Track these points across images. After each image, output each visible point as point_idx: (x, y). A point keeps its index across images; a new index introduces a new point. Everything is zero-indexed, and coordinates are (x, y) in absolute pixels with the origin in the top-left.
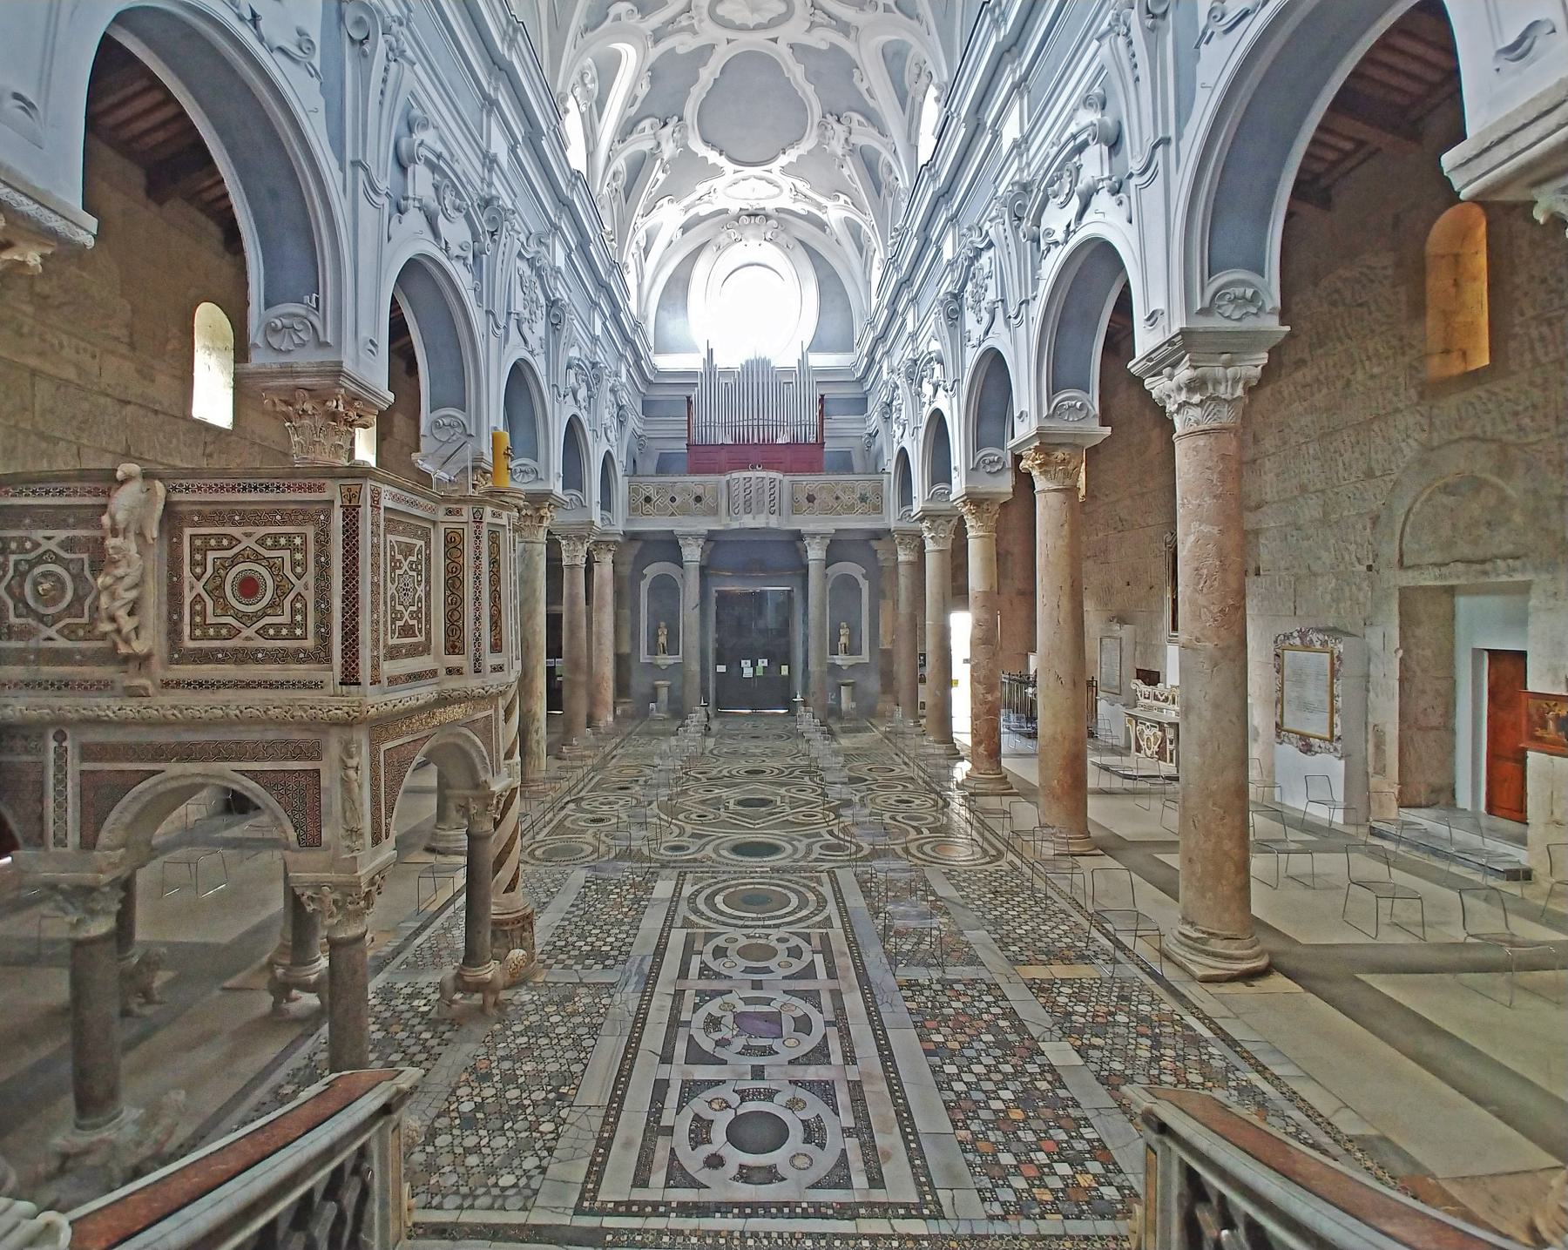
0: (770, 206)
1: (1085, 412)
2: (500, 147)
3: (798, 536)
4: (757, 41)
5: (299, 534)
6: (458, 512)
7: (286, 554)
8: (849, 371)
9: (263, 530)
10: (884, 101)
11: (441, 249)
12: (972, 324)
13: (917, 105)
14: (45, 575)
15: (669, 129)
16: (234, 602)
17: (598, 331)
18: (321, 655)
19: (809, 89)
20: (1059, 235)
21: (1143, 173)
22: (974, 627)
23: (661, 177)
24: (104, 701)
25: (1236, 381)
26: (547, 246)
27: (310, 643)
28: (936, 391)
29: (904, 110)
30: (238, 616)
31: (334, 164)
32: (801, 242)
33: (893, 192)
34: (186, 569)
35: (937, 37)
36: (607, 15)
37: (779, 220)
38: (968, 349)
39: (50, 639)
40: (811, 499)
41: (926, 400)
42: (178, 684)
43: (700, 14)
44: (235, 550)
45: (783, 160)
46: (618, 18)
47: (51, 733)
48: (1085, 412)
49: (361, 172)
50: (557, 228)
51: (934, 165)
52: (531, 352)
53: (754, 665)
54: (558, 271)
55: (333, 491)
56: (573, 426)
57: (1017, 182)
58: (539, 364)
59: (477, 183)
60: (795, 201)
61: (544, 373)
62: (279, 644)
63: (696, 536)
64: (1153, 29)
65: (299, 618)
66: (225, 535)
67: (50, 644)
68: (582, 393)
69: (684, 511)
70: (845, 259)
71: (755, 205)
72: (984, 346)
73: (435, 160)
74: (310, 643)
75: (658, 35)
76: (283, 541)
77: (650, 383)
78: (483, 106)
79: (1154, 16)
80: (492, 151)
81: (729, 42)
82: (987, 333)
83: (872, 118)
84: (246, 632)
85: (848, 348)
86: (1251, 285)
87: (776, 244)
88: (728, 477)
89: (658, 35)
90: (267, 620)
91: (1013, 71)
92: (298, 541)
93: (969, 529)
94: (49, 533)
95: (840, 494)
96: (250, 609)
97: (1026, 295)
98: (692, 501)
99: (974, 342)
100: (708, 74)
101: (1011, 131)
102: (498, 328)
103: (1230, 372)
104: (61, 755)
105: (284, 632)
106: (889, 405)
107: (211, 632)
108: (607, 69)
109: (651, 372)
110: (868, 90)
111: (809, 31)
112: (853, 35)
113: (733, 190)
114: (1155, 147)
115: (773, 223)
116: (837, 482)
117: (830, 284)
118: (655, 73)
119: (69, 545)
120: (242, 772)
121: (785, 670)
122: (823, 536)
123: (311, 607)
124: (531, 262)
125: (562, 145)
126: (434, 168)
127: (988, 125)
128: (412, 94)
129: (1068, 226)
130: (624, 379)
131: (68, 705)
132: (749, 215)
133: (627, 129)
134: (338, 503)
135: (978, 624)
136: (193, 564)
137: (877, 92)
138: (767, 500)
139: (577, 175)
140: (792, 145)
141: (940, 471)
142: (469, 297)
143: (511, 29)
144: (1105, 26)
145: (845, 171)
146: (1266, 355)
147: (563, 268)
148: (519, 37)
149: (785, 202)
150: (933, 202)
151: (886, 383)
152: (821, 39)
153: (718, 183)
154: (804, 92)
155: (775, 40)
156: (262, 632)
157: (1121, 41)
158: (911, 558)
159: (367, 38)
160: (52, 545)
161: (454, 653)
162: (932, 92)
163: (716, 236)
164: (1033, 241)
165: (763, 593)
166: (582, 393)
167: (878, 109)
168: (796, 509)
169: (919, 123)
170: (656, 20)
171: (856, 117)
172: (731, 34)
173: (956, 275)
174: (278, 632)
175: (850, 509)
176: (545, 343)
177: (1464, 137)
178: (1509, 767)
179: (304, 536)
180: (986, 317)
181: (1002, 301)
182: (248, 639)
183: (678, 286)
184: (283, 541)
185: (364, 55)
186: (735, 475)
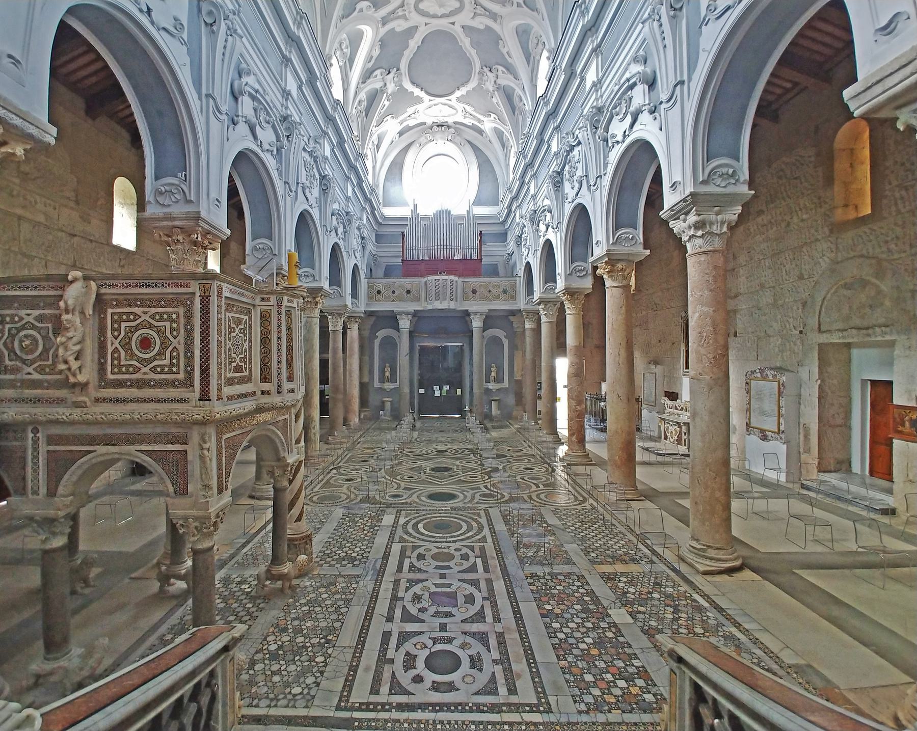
0: (450, 120)
1: (634, 241)
2: (292, 86)
3: (467, 313)
4: (443, 24)
5: (175, 313)
6: (268, 300)
8: (496, 217)
9: (154, 310)
11: (258, 146)
13: (536, 62)
15: (391, 75)
16: (137, 352)
17: (350, 194)
18: (188, 383)
19: (473, 52)
20: (619, 138)
21: (668, 101)
22: (570, 367)
23: (387, 103)
24: (61, 410)
25: (723, 223)
26: (320, 144)
27: (181, 376)
28: (547, 229)
29: (528, 64)
30: (139, 360)
31: (196, 96)
32: (469, 142)
33: (522, 112)
34: (109, 332)
35: (548, 22)
36: (355, 9)
37: (456, 129)
38: (566, 204)
39: (29, 374)
40: (474, 292)
41: (542, 234)
42: (104, 400)
44: (138, 322)
45: (458, 94)
46: (361, 10)
47: (30, 428)
48: (634, 241)
50: (326, 133)
51: (546, 96)
54: (327, 158)
55: (195, 287)
56: (335, 249)
57: (594, 107)
58: (315, 213)
59: (279, 107)
60: (465, 117)
61: (318, 218)
62: (163, 376)
63: (407, 314)
65: (175, 361)
66: (131, 313)
67: (29, 377)
68: (341, 230)
69: (400, 299)
70: (494, 152)
71: (441, 120)
72: (576, 202)
73: (254, 93)
74: (181, 376)
75: (385, 20)
76: (165, 316)
77: (380, 224)
78: (283, 62)
79: (675, 10)
81: (426, 24)
82: (577, 194)
83: (510, 69)
84: (144, 370)
85: (496, 204)
86: (731, 167)
87: (454, 143)
88: (426, 279)
89: (385, 20)
90: (156, 363)
91: (593, 42)
92: (174, 316)
93: (567, 310)
94: (29, 312)
95: (491, 289)
96: (146, 356)
97: (600, 172)
98: (404, 293)
99: (570, 200)
100: (414, 43)
101: (591, 77)
102: (291, 192)
103: (719, 217)
104: (36, 441)
105: (166, 369)
106: (520, 237)
108: (355, 41)
109: (381, 218)
110: (508, 53)
111: (473, 18)
112: (499, 20)
113: (429, 111)
114: (676, 86)
115: (452, 130)
116: (489, 282)
117: (485, 166)
118: (383, 43)
119: (40, 319)
120: (142, 452)
121: (459, 392)
122: (482, 313)
123: (182, 355)
124: (311, 153)
125: (329, 85)
126: (254, 98)
127: (578, 73)
128: (241, 55)
129: (625, 132)
130: (365, 222)
131: (40, 412)
132: (438, 126)
133: (367, 75)
134: (198, 294)
135: (572, 365)
136: (113, 330)
137: (513, 54)
138: (449, 292)
139: (337, 102)
140: (463, 85)
141: (550, 276)
142: (274, 174)
143: (299, 17)
144: (646, 15)
145: (494, 100)
146: (741, 208)
147: (329, 157)
149: (459, 118)
150: (546, 118)
151: (518, 224)
152: (480, 23)
153: (420, 107)
154: (470, 54)
155: (453, 24)
156: (153, 370)
158: (533, 326)
160: (30, 319)
161: (265, 382)
162: (545, 54)
163: (419, 138)
165: (446, 347)
166: (341, 230)
167: (513, 63)
168: (465, 298)
169: (537, 72)
170: (384, 12)
171: (501, 68)
172: (427, 20)
173: (559, 161)
174: (163, 370)
175: (497, 297)
176: (319, 201)
177: (856, 80)
179: (178, 314)
180: (577, 186)
181: (586, 176)
182: (145, 373)
183: (396, 167)
184: (165, 316)
185: (213, 32)
186: (430, 278)
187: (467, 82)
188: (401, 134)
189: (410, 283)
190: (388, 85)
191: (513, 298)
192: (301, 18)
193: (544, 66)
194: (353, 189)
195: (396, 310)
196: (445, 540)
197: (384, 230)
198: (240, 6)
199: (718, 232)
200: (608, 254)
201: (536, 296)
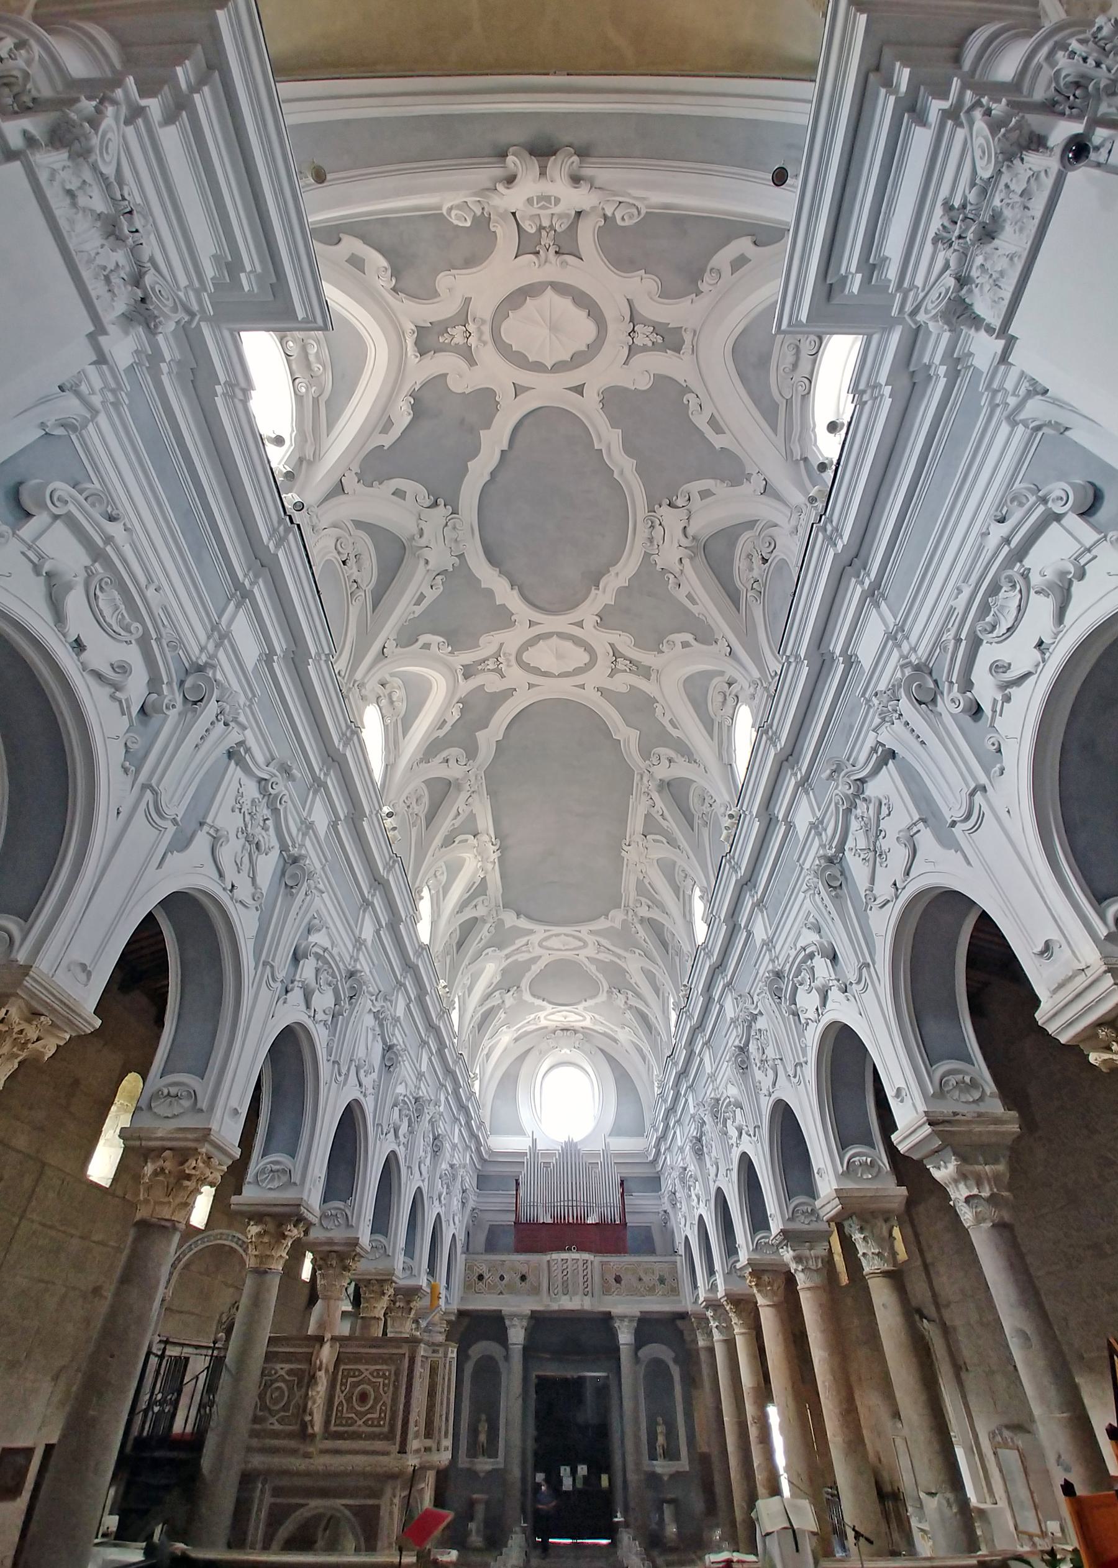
1: (876, 1169)
2: (368, 932)
3: (607, 1318)
7: (381, 1380)
8: (646, 1152)
10: (666, 894)
11: (309, 1017)
12: (807, 1001)
13: (687, 898)
15: (510, 993)
17: (424, 1068)
18: (389, 1437)
19: (600, 976)
21: (968, 817)
23: (503, 1016)
24: (292, 1460)
26: (391, 1002)
28: (741, 1134)
29: (658, 997)
30: (357, 1413)
31: (252, 964)
32: (602, 1050)
33: (679, 952)
34: (338, 1387)
35: (694, 859)
36: (417, 640)
37: (583, 1033)
38: (762, 1097)
40: (618, 1280)
41: (733, 1141)
43: (508, 660)
44: (360, 1378)
47: (261, 1478)
48: (876, 1169)
49: (336, 1066)
50: (401, 985)
51: (771, 726)
52: (365, 1096)
53: (574, 1472)
54: (398, 1020)
55: (405, 1350)
56: (390, 1167)
58: (369, 1105)
59: (347, 958)
61: (372, 1109)
63: (520, 1317)
64: (837, 896)
65: (383, 1415)
67: (272, 1427)
68: (404, 1129)
69: (511, 1289)
70: (634, 1065)
71: (566, 1025)
73: (100, 543)
74: (386, 1429)
75: (507, 957)
77: (485, 1161)
78: (362, 905)
79: (835, 888)
80: (363, 937)
82: (774, 1084)
83: (638, 995)
84: (360, 1422)
85: (640, 1132)
86: (867, 1156)
87: (583, 1051)
88: (548, 1257)
89: (507, 957)
90: (369, 1416)
91: (665, 1144)
93: (735, 1326)
95: (643, 1276)
96: (363, 1409)
97: (799, 1059)
98: (518, 1280)
99: (765, 1091)
101: (760, 933)
102: (274, 980)
104: (262, 1492)
106: (699, 1140)
107: (344, 1422)
108: (454, 870)
109: (486, 1152)
110: (671, 721)
112: (653, 676)
113: (551, 1017)
114: (972, 794)
115: (580, 1036)
116: (639, 1263)
117: (624, 1081)
118: (504, 972)
119: (290, 1372)
121: (605, 1480)
122: (631, 1318)
125: (415, 920)
126: (318, 957)
127: (780, 818)
128: (317, 912)
129: (817, 1009)
130: (442, 1109)
131: (276, 1461)
132: (562, 1030)
133: (487, 997)
134: (407, 1355)
136: (342, 1384)
138: (581, 1280)
139: (423, 947)
141: (758, 1220)
142: (321, 1053)
143: (281, 528)
144: (727, 1058)
147: (369, 943)
148: (424, 952)
149: (587, 1023)
150: (776, 769)
151: (693, 1116)
152: (623, 682)
153: (542, 1014)
155: (582, 687)
157: (898, 725)
159: (201, 700)
162: (697, 892)
164: (794, 1014)
165: (582, 1379)
166: (404, 1129)
168: (606, 1291)
169: (820, 364)
170: (467, 657)
172: (550, 952)
173: (740, 1031)
175: (651, 1290)
176: (376, 1087)
177: (897, 1129)
178: (890, 1504)
179: (390, 1371)
180: (770, 1073)
181: (781, 1059)
182: (360, 1426)
183: (509, 1081)
185: (292, 894)
186: (555, 1256)
188: (516, 1040)
189: (527, 1262)
190: (506, 1001)
191: (675, 1291)
192: (394, 862)
193: (699, 907)
195: (506, 1310)
197: (492, 1170)
198: (254, 696)
199: (814, 1267)
200: (750, 1263)
201: (776, 1226)
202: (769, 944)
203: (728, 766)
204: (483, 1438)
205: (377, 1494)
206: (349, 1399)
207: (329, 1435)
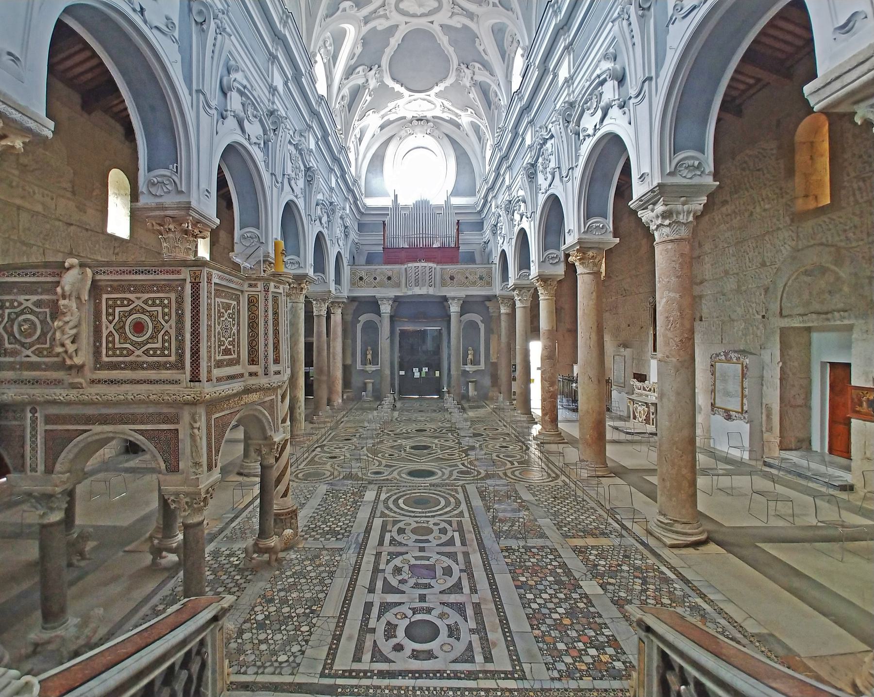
0: (429, 115)
1: (605, 230)
2: (278, 82)
3: (445, 299)
4: (422, 23)
5: (166, 298)
6: (256, 286)
8: (473, 207)
9: (146, 296)
10: (493, 56)
13: (511, 59)
14: (25, 321)
15: (373, 72)
16: (130, 336)
17: (334, 185)
18: (179, 365)
19: (451, 50)
20: (590, 131)
21: (637, 96)
22: (543, 350)
23: (369, 98)
24: (58, 391)
25: (689, 212)
26: (305, 137)
27: (173, 359)
28: (522, 218)
29: (504, 61)
30: (133, 343)
31: (186, 92)
32: (447, 135)
33: (498, 107)
34: (104, 317)
35: (522, 21)
36: (339, 8)
37: (434, 123)
38: (540, 195)
39: (28, 356)
40: (452, 278)
41: (516, 223)
42: (99, 381)
43: (390, 8)
44: (131, 307)
45: (437, 89)
46: (344, 10)
47: (28, 409)
48: (605, 230)
49: (201, 96)
50: (311, 127)
51: (521, 92)
53: (420, 371)
54: (311, 151)
55: (186, 274)
56: (319, 237)
58: (300, 203)
60: (443, 112)
61: (303, 208)
62: (156, 359)
63: (388, 299)
65: (166, 344)
66: (125, 298)
67: (28, 359)
68: (325, 219)
69: (382, 285)
70: (471, 145)
71: (421, 114)
73: (242, 89)
74: (173, 359)
75: (367, 19)
76: (158, 302)
77: (363, 214)
78: (269, 59)
79: (643, 9)
81: (406, 23)
82: (550, 185)
83: (486, 66)
84: (137, 353)
85: (473, 194)
86: (697, 159)
87: (433, 136)
88: (406, 266)
89: (367, 19)
90: (149, 346)
91: (565, 40)
92: (166, 302)
93: (540, 295)
94: (27, 297)
95: (468, 275)
96: (140, 340)
97: (572, 164)
98: (386, 280)
99: (543, 191)
100: (395, 41)
101: (563, 73)
102: (278, 183)
104: (34, 421)
105: (158, 352)
106: (496, 226)
108: (339, 39)
109: (363, 207)
110: (484, 50)
111: (451, 17)
112: (475, 19)
113: (409, 106)
114: (644, 82)
115: (431, 124)
116: (467, 269)
117: (463, 159)
118: (365, 41)
120: (135, 431)
121: (437, 374)
122: (459, 299)
123: (173, 338)
124: (296, 146)
125: (313, 81)
126: (242, 94)
127: (551, 70)
128: (230, 52)
129: (596, 126)
130: (348, 211)
131: (38, 393)
132: (417, 120)
133: (350, 72)
134: (188, 280)
135: (545, 348)
136: (108, 314)
137: (489, 51)
138: (427, 279)
139: (321, 97)
140: (441, 81)
141: (524, 263)
142: (261, 166)
143: (285, 16)
145: (471, 96)
146: (706, 198)
147: (314, 150)
149: (438, 112)
150: (520, 113)
151: (494, 213)
152: (458, 22)
153: (400, 102)
154: (448, 51)
155: (432, 22)
156: (146, 353)
158: (508, 311)
160: (29, 304)
161: (253, 364)
162: (520, 51)
163: (399, 132)
164: (576, 134)
165: (425, 331)
166: (325, 219)
167: (489, 61)
168: (443, 284)
169: (512, 69)
170: (366, 11)
171: (477, 65)
172: (407, 19)
173: (533, 153)
174: (155, 352)
175: (474, 284)
176: (304, 192)
177: (816, 77)
179: (169, 299)
180: (550, 177)
181: (559, 168)
182: (138, 356)
183: (378, 159)
184: (158, 302)
185: (203, 30)
186: (410, 265)
187: (445, 78)
188: (382, 127)
189: (391, 270)
190: (370, 81)
193: (519, 63)
194: (337, 180)
195: (378, 295)
196: (424, 515)
197: (366, 220)
201: (511, 282)
202: (569, 81)
203: (509, 82)
204: (369, 357)
205: (175, 419)
206: (120, 329)
207: (99, 365)
